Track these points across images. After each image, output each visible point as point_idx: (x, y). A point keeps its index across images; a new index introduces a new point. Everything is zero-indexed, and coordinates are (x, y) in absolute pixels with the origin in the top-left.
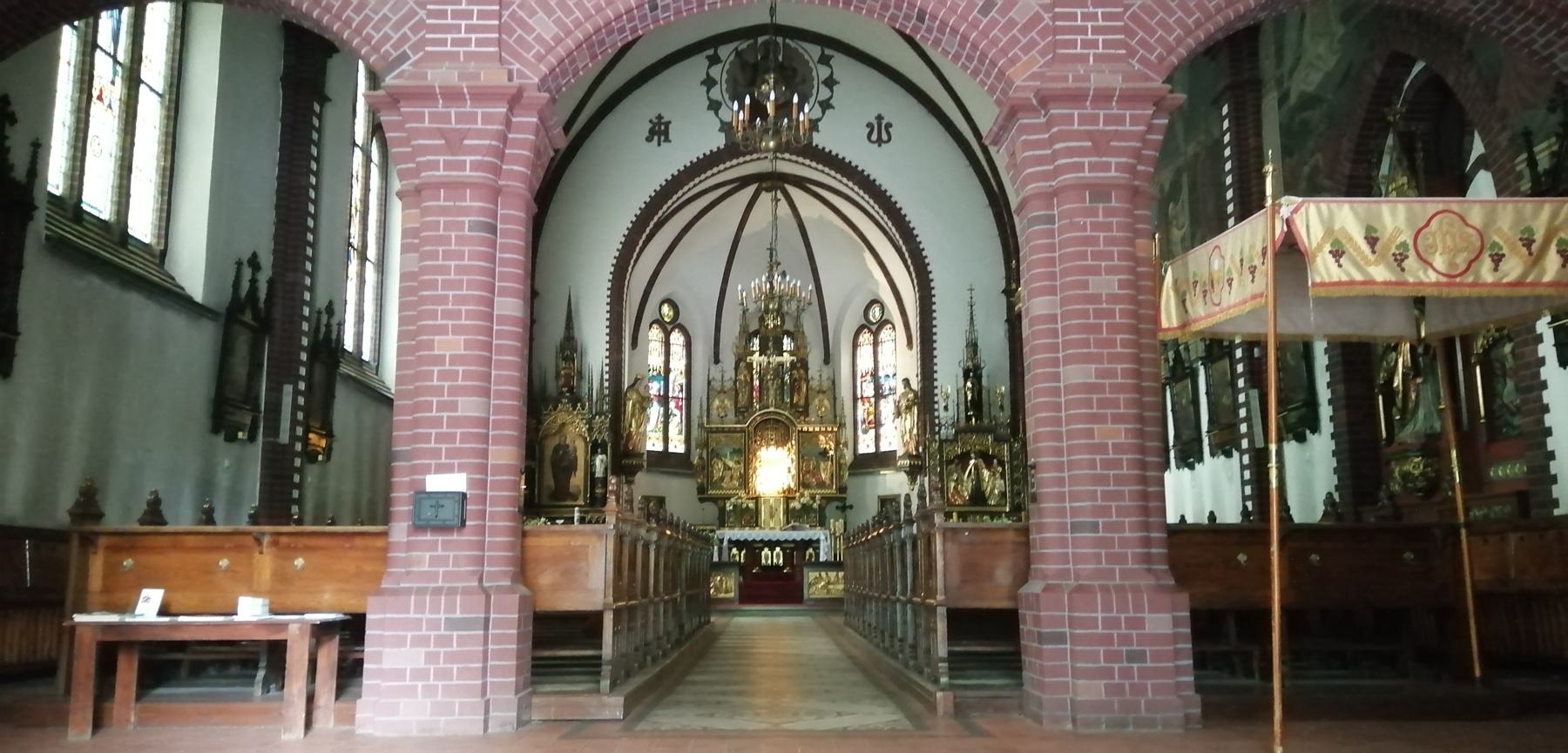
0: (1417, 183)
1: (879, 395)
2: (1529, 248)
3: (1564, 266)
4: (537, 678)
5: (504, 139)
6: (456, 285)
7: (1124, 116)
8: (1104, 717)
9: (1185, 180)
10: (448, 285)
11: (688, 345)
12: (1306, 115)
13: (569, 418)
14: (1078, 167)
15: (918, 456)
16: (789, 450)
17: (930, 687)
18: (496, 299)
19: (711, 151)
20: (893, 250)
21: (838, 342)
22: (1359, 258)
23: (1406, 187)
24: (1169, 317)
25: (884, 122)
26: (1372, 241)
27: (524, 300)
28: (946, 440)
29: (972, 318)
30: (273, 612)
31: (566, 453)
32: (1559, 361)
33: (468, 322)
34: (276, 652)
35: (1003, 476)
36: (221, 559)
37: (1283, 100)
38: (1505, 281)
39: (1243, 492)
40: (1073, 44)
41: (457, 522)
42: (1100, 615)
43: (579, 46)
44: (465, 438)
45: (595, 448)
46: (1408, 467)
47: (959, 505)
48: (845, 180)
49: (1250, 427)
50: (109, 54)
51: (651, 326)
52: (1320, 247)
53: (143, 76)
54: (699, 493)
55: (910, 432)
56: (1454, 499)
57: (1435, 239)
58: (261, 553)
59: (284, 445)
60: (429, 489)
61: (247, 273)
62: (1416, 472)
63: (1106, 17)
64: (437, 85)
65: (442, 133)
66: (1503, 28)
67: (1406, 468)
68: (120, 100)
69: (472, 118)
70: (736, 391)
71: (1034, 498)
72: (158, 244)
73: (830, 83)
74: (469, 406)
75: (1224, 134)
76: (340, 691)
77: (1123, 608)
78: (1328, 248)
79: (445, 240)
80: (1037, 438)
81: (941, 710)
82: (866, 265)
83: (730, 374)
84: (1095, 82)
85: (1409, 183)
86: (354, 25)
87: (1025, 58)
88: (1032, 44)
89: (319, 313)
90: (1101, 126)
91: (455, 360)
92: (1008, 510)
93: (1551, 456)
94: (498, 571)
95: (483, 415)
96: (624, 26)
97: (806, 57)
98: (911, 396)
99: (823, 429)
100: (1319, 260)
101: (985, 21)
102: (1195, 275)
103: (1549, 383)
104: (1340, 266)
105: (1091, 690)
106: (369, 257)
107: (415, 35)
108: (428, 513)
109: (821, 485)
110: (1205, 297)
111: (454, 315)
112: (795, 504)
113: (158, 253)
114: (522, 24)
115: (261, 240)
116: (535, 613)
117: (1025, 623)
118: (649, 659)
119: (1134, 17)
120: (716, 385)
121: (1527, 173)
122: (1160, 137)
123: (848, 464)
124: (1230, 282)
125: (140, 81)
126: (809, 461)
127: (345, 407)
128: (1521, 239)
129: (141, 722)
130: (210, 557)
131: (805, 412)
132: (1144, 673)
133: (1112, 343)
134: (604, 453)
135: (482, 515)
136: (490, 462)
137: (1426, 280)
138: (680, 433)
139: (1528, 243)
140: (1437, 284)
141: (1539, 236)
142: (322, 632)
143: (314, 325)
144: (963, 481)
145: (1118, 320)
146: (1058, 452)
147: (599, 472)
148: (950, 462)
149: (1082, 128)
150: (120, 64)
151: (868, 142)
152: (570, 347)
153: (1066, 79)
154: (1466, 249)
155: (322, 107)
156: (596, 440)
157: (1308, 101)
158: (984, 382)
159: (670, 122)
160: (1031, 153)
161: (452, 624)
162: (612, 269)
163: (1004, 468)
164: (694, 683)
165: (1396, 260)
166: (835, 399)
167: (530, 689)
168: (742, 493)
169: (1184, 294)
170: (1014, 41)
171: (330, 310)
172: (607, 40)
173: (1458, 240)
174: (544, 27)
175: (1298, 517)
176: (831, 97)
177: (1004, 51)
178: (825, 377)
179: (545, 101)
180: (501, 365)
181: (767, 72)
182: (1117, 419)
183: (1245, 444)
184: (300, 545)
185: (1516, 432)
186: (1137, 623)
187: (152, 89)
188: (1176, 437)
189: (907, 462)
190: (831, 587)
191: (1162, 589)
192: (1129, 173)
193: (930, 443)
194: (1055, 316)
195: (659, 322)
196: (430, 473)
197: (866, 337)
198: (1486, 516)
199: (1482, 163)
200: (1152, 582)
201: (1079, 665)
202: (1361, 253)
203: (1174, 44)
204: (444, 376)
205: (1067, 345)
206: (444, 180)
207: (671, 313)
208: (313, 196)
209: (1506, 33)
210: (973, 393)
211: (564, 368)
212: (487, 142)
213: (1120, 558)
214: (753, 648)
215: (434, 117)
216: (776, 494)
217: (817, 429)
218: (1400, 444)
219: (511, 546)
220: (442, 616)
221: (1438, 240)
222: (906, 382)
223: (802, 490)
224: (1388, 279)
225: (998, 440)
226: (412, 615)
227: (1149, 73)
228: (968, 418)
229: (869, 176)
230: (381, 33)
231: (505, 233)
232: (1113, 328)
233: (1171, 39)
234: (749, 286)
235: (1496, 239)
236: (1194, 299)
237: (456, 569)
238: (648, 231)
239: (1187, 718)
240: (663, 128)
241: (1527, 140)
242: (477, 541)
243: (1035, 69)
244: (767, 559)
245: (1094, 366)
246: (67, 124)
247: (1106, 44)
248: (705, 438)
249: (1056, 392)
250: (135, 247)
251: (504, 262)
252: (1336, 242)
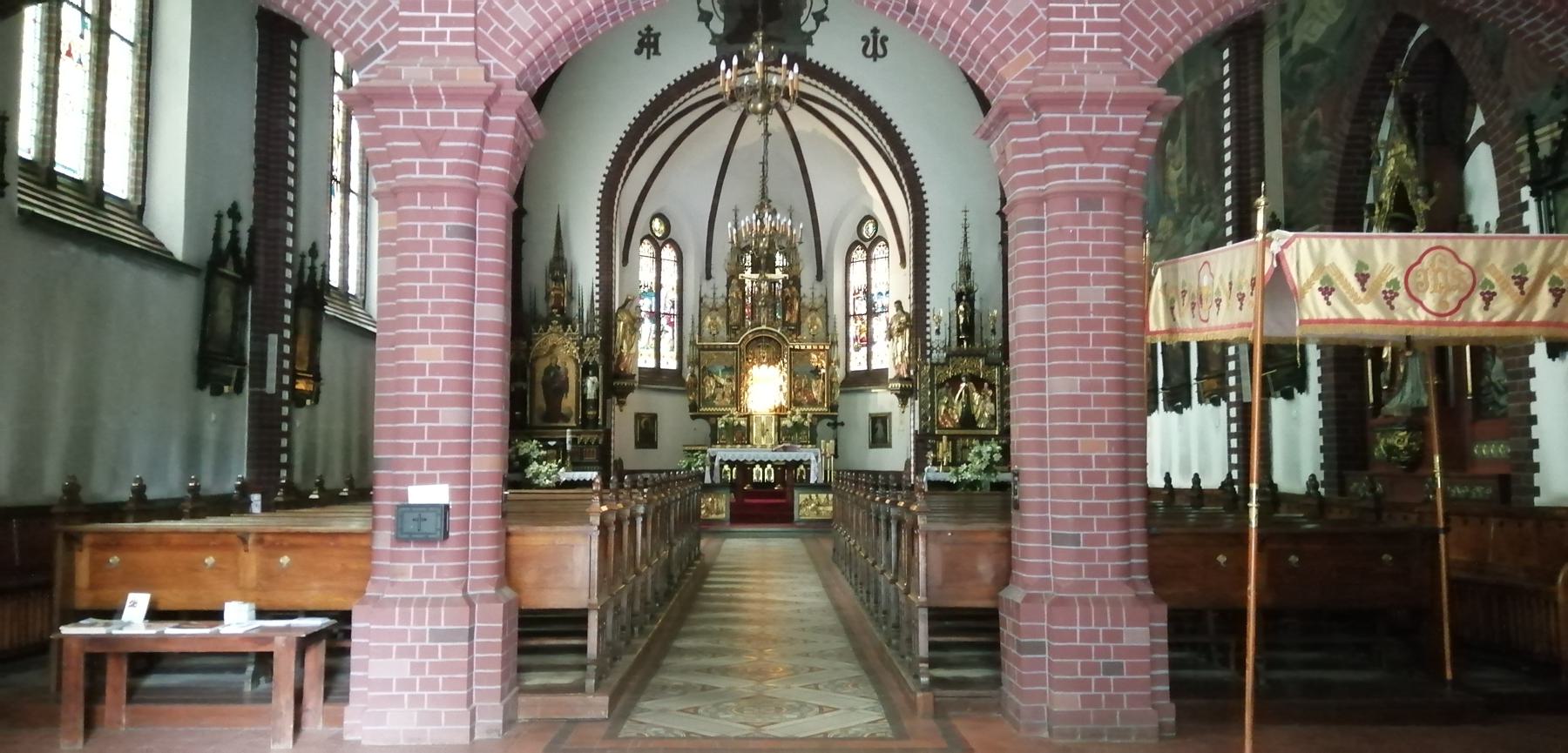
0: (1416, 152)
1: (871, 313)
2: (1521, 287)
3: (1555, 305)
4: (527, 660)
5: (481, 139)
6: (436, 292)
7: (1117, 120)
8: (1079, 727)
9: (1183, 118)
10: (426, 292)
11: (680, 261)
12: (1308, 67)
13: (560, 340)
14: (1070, 173)
15: (909, 379)
16: (781, 368)
17: (910, 681)
18: (476, 304)
19: (702, 65)
21: (831, 259)
22: (1348, 296)
23: (1405, 155)
24: (1157, 320)
26: (1362, 278)
27: (505, 304)
28: (937, 364)
29: (966, 241)
30: (261, 614)
31: (557, 375)
32: (1548, 352)
33: (447, 331)
34: (264, 661)
35: (993, 399)
36: (207, 556)
37: (1286, 47)
38: (1495, 320)
39: (1229, 444)
40: (1067, 41)
41: (439, 534)
42: (1078, 628)
43: (558, 39)
44: (447, 448)
45: (586, 370)
46: (1393, 441)
47: (949, 429)
48: (839, 96)
49: (1238, 381)
50: (77, 7)
51: (642, 241)
52: (1309, 284)
53: (113, 26)
54: (691, 411)
55: (902, 355)
56: (1434, 503)
57: (1426, 278)
58: (246, 551)
59: (272, 395)
60: (412, 501)
61: (227, 224)
62: (1401, 446)
63: (1102, 13)
64: (411, 86)
65: (417, 135)
66: (1511, 21)
67: (1390, 441)
68: (90, 53)
69: (448, 119)
70: (728, 308)
71: (1017, 507)
72: (136, 198)
74: (450, 417)
75: (1224, 79)
76: (327, 693)
77: (1101, 621)
78: (1317, 285)
79: (423, 246)
80: (1021, 446)
81: (920, 710)
82: (860, 180)
83: (722, 291)
84: (1089, 85)
85: (1408, 151)
86: (324, 16)
87: (1017, 56)
88: (1025, 41)
89: (303, 256)
90: (1093, 131)
91: (436, 369)
92: (997, 433)
93: (1535, 444)
94: (482, 581)
95: (465, 425)
96: (604, 15)
98: (903, 319)
99: (815, 347)
100: (1308, 296)
101: (978, 15)
102: (1184, 284)
103: (1537, 395)
104: (1329, 304)
105: (1066, 701)
106: (352, 188)
107: (388, 27)
108: (411, 526)
109: (813, 403)
110: (1193, 309)
111: (434, 323)
112: (786, 422)
113: (135, 209)
114: (499, 15)
115: (240, 188)
116: (521, 612)
117: (1005, 627)
118: (636, 629)
119: (1130, 12)
120: (709, 302)
121: (1527, 157)
122: (1154, 140)
123: (840, 382)
124: (1218, 302)
125: (109, 32)
126: (800, 379)
127: (332, 348)
128: (1514, 277)
129: (131, 723)
130: (196, 555)
131: (796, 329)
132: (1121, 686)
133: (1098, 355)
134: (596, 374)
135: (465, 524)
136: (473, 470)
137: (1415, 318)
138: (672, 349)
139: (1520, 281)
140: (1426, 323)
141: (1532, 275)
142: (305, 644)
143: (296, 272)
144: (953, 404)
145: (1105, 331)
146: (1041, 462)
147: (590, 393)
148: (940, 385)
149: (1074, 133)
150: (88, 15)
152: (560, 268)
153: (1058, 81)
154: (1457, 287)
155: (299, 45)
156: (587, 362)
157: (1312, 53)
158: (977, 305)
159: (659, 34)
160: (1021, 156)
161: (437, 636)
162: (602, 187)
163: (994, 391)
164: (681, 652)
165: (1386, 298)
166: (827, 316)
167: (516, 689)
168: (733, 411)
169: (1173, 301)
170: (1007, 37)
171: (314, 252)
172: (587, 29)
173: (1449, 278)
174: (522, 19)
175: (1279, 477)
176: (826, 8)
177: (995, 49)
178: (817, 294)
179: (523, 100)
180: (481, 372)
181: (756, 29)
182: (1101, 432)
183: (1233, 397)
184: (285, 544)
185: (1502, 411)
186: (1114, 636)
187: (123, 39)
188: (1165, 379)
189: (898, 385)
190: (821, 508)
191: (1141, 599)
192: (1121, 180)
193: (922, 366)
194: (1042, 324)
195: (651, 237)
196: (411, 484)
197: (859, 254)
198: (1468, 494)
199: (1482, 135)
200: (1130, 594)
201: (1056, 677)
202: (1351, 290)
203: (1171, 40)
204: (424, 385)
205: (1053, 356)
206: (420, 184)
207: (662, 228)
208: (295, 64)
209: (1512, 26)
210: (965, 316)
211: (554, 289)
212: (465, 144)
213: (1101, 571)
214: (736, 621)
215: (409, 118)
216: (767, 412)
217: (809, 347)
218: (1387, 416)
219: (496, 554)
220: (427, 628)
221: (1430, 278)
222: (899, 304)
223: (793, 408)
224: (1377, 318)
225: (989, 364)
226: (397, 626)
227: (1145, 71)
228: (960, 342)
229: (863, 92)
230: (353, 25)
231: (485, 237)
232: (1100, 340)
233: (1168, 35)
234: (742, 222)
235: (1489, 276)
236: (1182, 309)
237: (440, 580)
238: (637, 147)
239: (1161, 727)
240: (652, 40)
241: (1529, 123)
242: (463, 459)
243: (1028, 67)
244: (758, 475)
245: (1079, 378)
246: (36, 84)
247: (1102, 42)
248: (698, 355)
249: (1041, 402)
250: (113, 205)
251: (484, 267)
252: (1326, 279)
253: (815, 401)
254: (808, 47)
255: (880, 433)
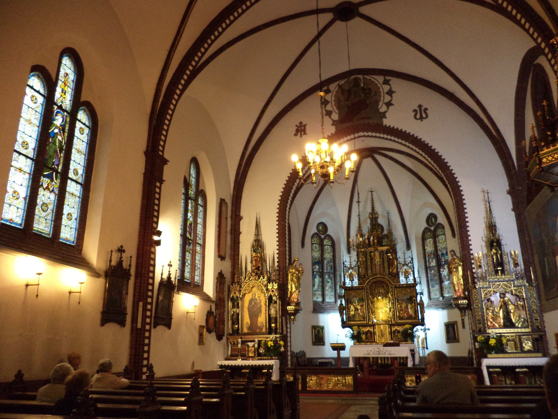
20: (436, 178)
25: (423, 108)
31: (255, 303)
60: (140, 327)
73: (390, 93)
97: (376, 82)
126: (401, 303)
151: (414, 119)
176: (391, 100)
240: (303, 128)
253: (411, 316)
254: (384, 119)
255: (451, 333)
